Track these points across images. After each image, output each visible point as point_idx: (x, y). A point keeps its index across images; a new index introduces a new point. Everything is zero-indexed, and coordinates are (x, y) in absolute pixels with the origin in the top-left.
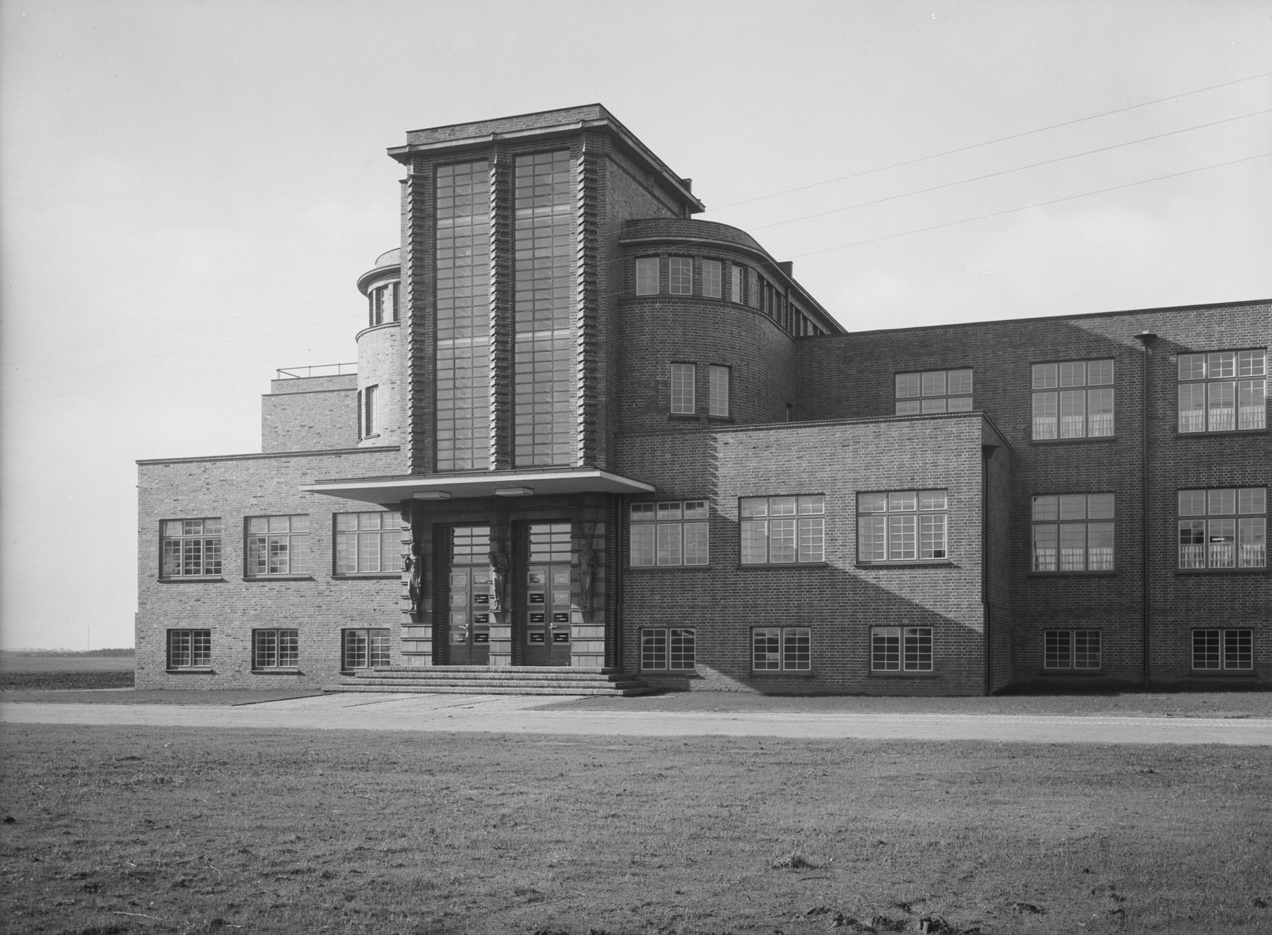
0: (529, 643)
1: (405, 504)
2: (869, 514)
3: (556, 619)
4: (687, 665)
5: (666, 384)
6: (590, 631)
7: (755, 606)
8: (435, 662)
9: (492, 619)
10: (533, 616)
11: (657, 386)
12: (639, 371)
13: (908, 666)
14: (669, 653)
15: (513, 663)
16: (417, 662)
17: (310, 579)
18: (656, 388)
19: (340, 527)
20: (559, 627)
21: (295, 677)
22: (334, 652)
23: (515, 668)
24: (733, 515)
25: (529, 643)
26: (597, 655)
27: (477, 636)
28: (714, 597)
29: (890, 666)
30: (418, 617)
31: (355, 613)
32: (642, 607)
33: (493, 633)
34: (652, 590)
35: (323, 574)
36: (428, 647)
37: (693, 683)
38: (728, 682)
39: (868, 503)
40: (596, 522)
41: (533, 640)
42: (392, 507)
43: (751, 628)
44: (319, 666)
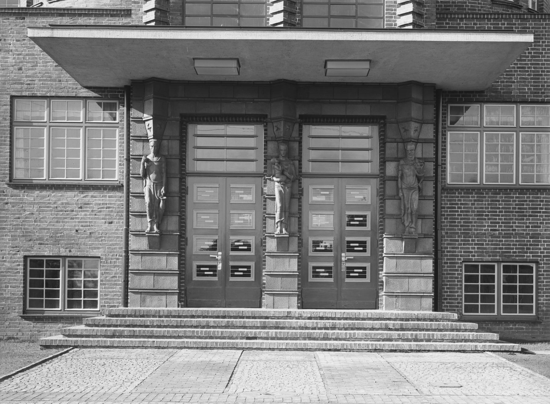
0: (311, 279)
2: (29, 124)
6: (411, 265)
8: (436, 308)
9: (271, 245)
13: (506, 309)
14: (498, 293)
15: (302, 306)
23: (439, 314)
25: (311, 279)
27: (235, 268)
30: (158, 243)
31: (45, 235)
32: (466, 235)
36: (172, 283)
39: (24, 110)
41: (316, 275)
43: (537, 263)
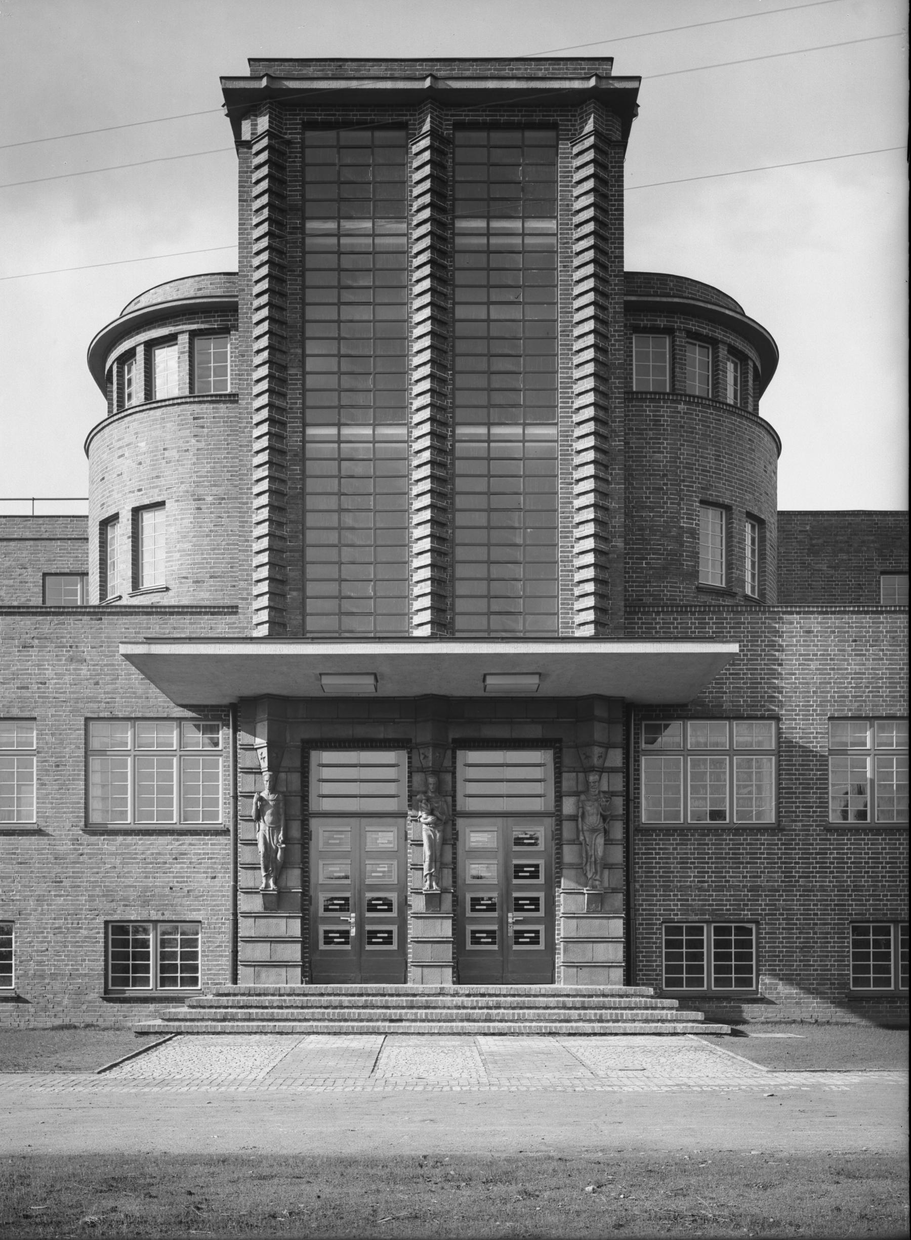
1: (228, 705)
3: (519, 908)
4: (742, 982)
5: (694, 534)
7: (857, 888)
9: (418, 904)
10: (476, 901)
11: (680, 535)
12: (651, 509)
14: (708, 962)
15: (458, 980)
16: (271, 980)
17: (39, 832)
18: (679, 540)
19: (95, 744)
20: (524, 921)
21: (10, 1006)
22: (93, 960)
23: (631, 989)
24: (819, 745)
26: (609, 966)
28: (788, 874)
29: (690, 982)
30: (275, 903)
31: (132, 894)
32: (667, 888)
33: (414, 929)
34: (683, 862)
35: (65, 828)
36: (294, 952)
37: (749, 1011)
38: (815, 1007)
40: (608, 746)
42: (209, 716)
44: (57, 985)
